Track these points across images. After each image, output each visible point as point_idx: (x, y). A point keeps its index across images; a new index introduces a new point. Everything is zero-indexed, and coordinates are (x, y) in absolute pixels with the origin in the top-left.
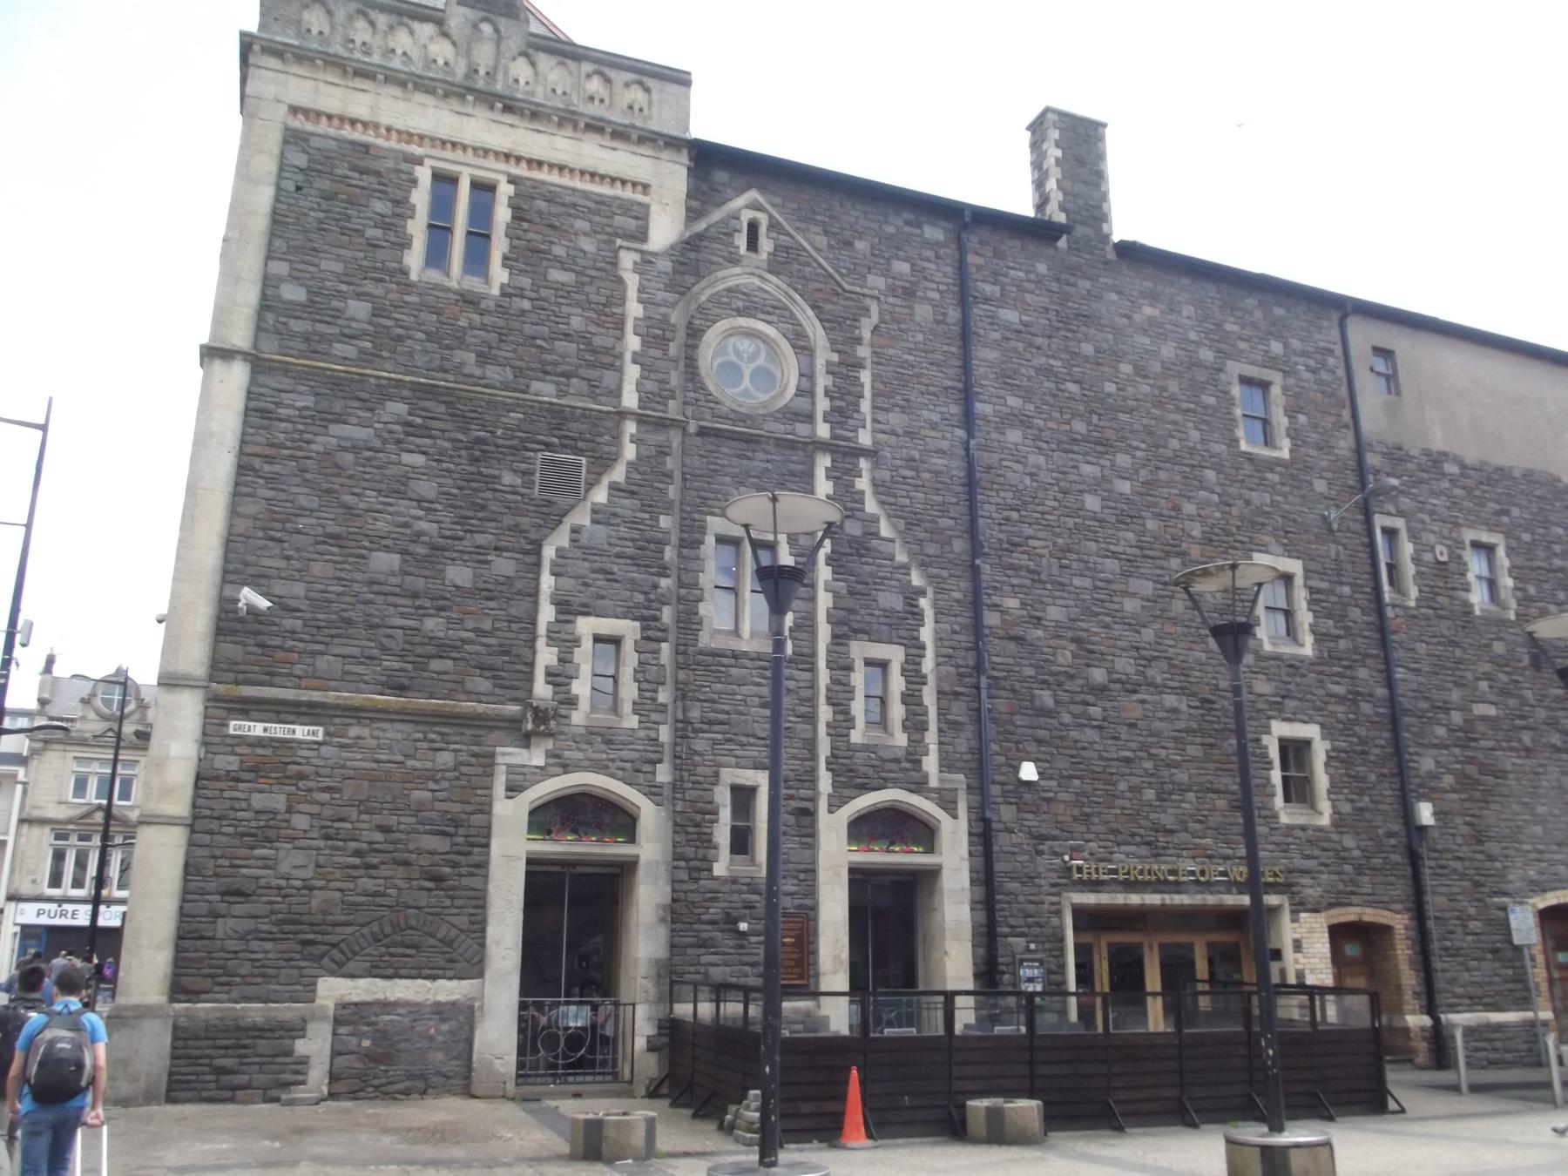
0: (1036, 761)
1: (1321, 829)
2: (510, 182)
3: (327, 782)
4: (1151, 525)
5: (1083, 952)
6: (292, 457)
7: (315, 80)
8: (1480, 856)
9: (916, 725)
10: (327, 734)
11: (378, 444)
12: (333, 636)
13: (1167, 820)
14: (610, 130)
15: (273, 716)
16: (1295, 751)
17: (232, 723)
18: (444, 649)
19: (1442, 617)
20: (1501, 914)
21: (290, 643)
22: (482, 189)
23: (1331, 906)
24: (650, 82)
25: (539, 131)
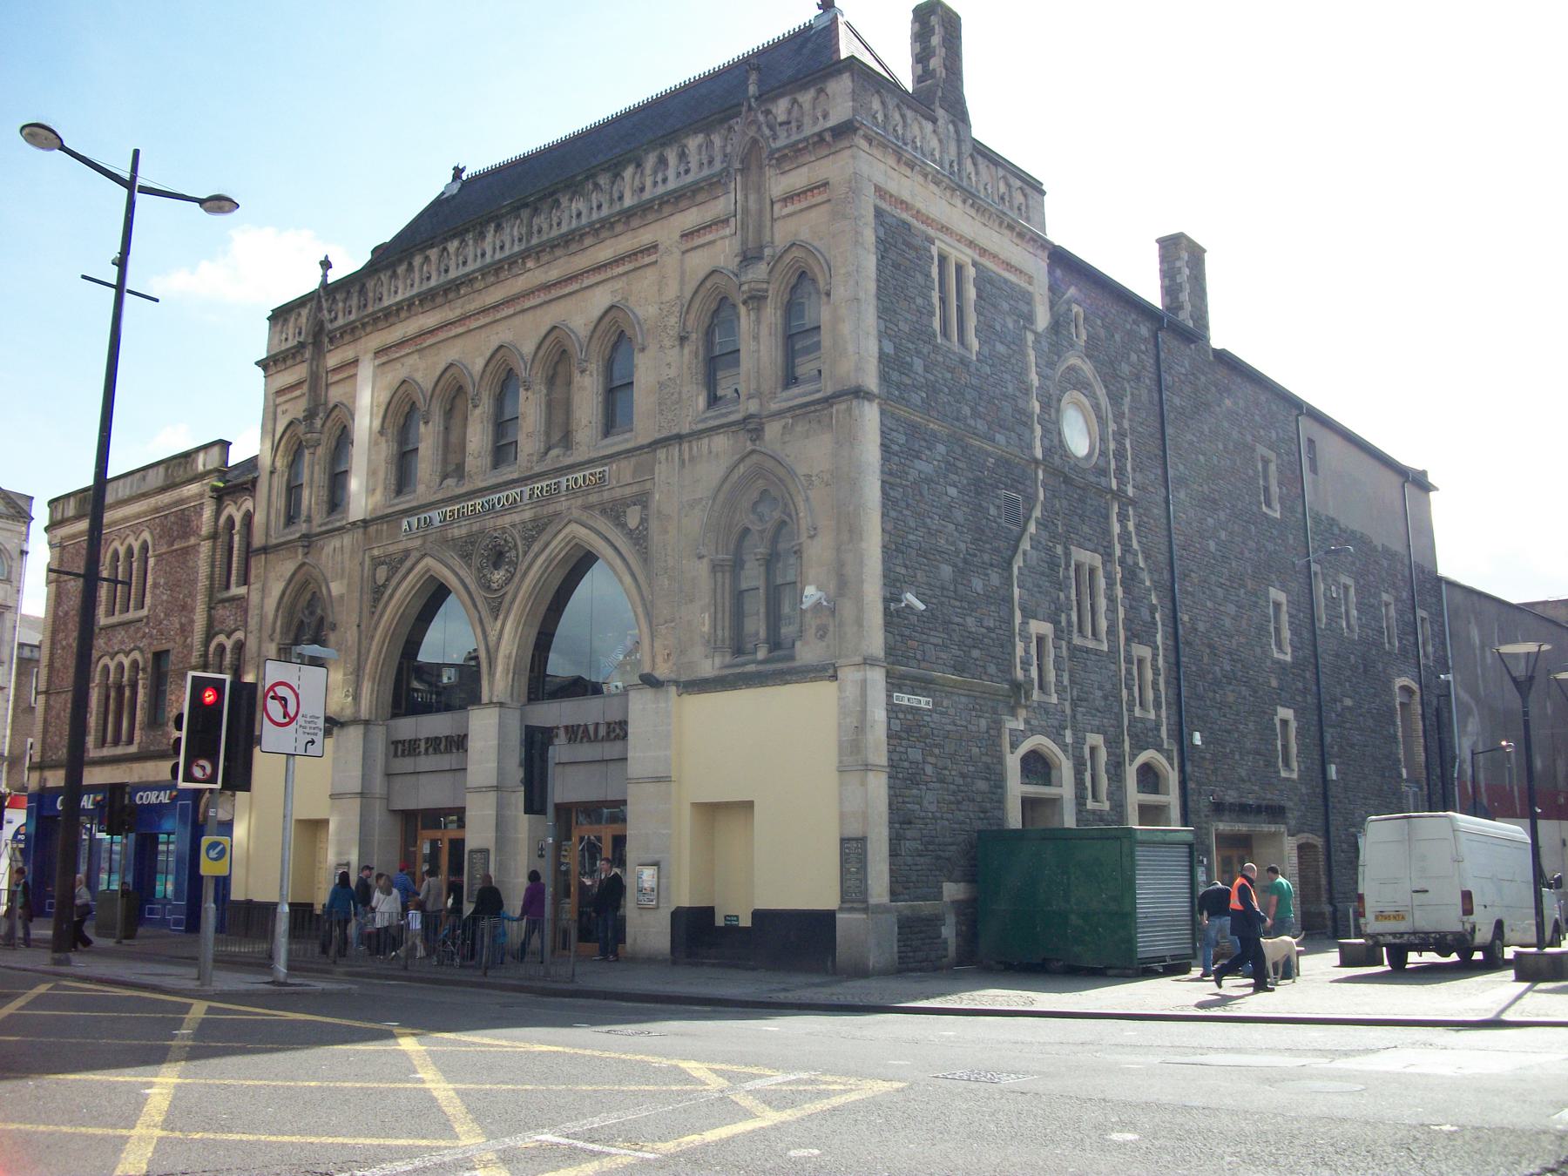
1: (1293, 781)
2: (973, 265)
9: (1157, 705)
14: (1017, 230)
16: (1285, 723)
23: (188, 547)
24: (1028, 190)
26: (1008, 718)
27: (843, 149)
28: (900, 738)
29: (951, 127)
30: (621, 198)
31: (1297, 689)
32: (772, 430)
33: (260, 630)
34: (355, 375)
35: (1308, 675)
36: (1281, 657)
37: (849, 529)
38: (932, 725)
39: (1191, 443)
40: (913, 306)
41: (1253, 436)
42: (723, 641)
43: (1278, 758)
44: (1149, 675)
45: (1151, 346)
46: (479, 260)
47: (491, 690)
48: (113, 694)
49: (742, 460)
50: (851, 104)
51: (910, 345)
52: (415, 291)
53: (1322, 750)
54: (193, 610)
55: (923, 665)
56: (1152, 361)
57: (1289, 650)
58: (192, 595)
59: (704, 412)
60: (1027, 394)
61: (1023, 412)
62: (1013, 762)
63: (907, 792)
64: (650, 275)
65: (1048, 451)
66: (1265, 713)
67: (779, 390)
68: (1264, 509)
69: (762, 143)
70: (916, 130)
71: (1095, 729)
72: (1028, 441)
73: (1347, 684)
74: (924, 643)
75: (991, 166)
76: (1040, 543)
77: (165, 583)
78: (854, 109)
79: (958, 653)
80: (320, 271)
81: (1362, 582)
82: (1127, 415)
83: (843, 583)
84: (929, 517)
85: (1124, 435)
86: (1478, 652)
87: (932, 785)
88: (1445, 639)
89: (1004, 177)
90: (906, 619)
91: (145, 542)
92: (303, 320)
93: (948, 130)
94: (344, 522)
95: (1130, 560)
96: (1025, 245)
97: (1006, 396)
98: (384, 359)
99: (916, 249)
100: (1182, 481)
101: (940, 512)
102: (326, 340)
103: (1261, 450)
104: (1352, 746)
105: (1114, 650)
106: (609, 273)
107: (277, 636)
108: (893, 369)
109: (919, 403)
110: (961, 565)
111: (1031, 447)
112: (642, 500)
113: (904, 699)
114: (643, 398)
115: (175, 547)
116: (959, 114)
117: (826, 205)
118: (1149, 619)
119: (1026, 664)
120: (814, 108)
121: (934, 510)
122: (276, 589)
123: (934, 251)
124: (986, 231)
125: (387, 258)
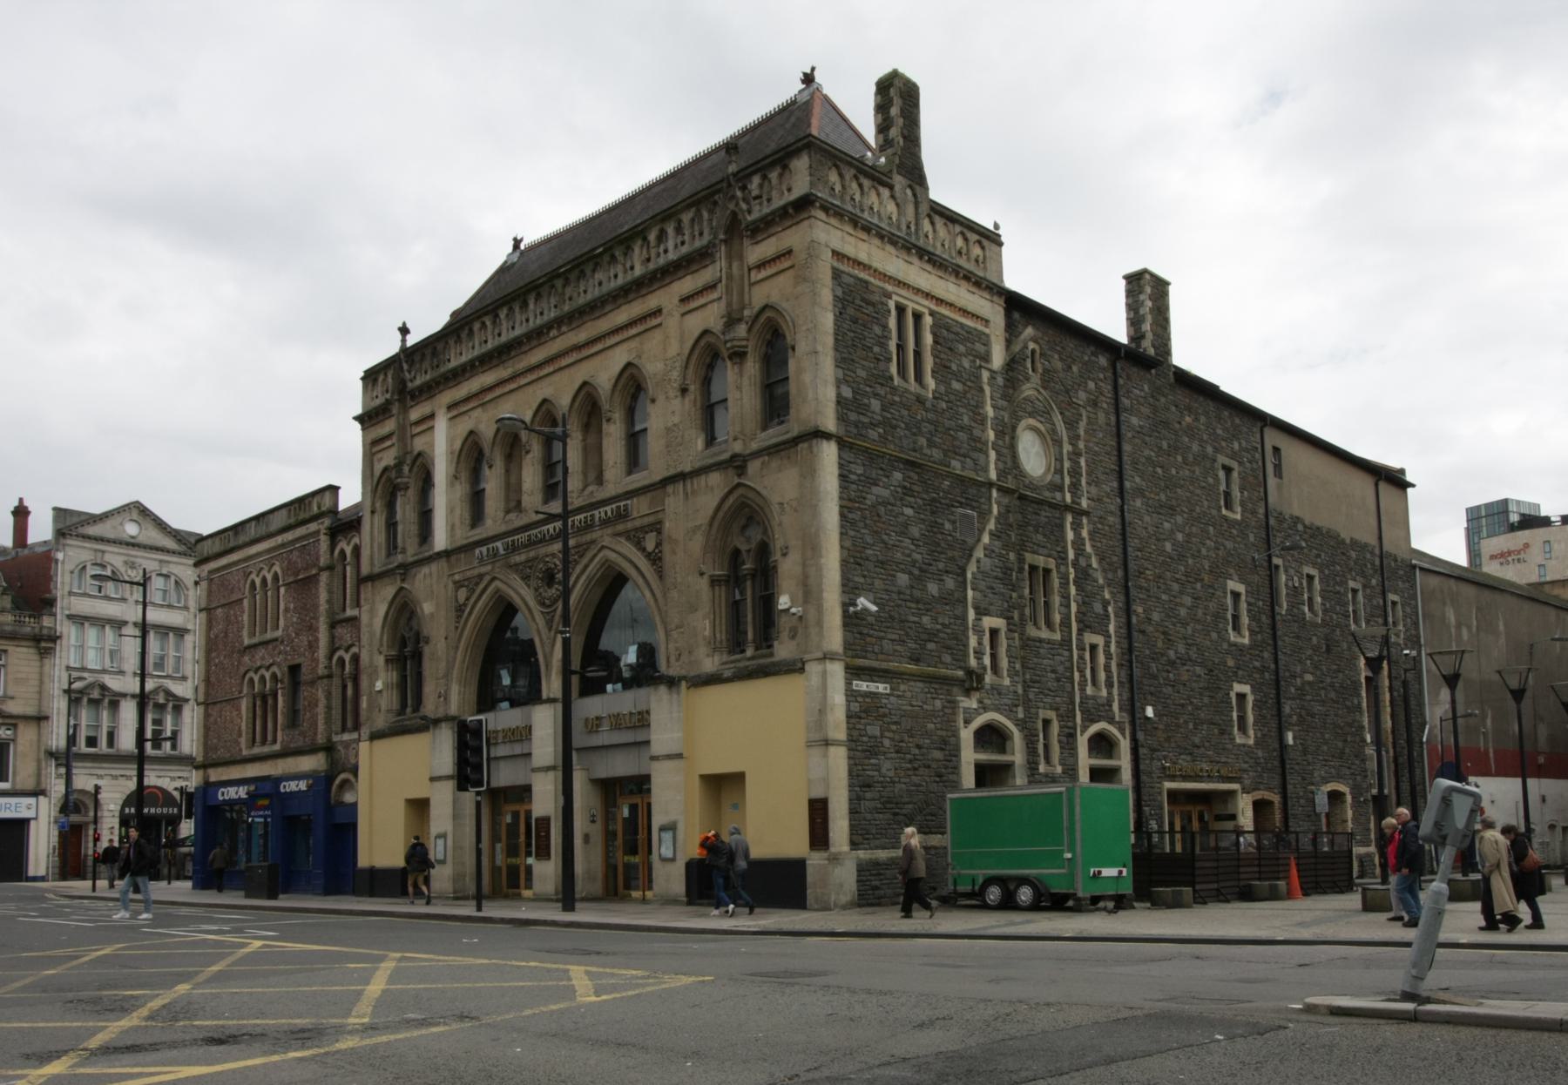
0: (1152, 705)
1: (1249, 747)
2: (930, 315)
3: (895, 719)
4: (1190, 561)
5: (1171, 814)
6: (859, 509)
7: (842, 230)
8: (1305, 763)
9: (1109, 685)
10: (891, 689)
11: (892, 500)
12: (888, 627)
13: (1197, 740)
15: (868, 677)
16: (1241, 697)
17: (854, 682)
18: (932, 636)
19: (1295, 621)
20: (1311, 795)
21: (872, 632)
22: (918, 317)
23: (1254, 790)
24: (985, 242)
25: (941, 277)
26: (962, 698)
27: (802, 220)
28: (860, 718)
29: (909, 192)
30: (632, 268)
31: (1255, 668)
32: (753, 467)
33: (370, 645)
34: (432, 427)
35: (1266, 655)
36: (1239, 640)
37: (812, 547)
38: (889, 706)
39: (1149, 459)
40: (870, 355)
41: (1215, 448)
42: (721, 642)
43: (1233, 726)
44: (1101, 659)
45: (1109, 374)
46: (524, 324)
47: (549, 689)
48: (258, 703)
49: (730, 492)
50: (808, 178)
51: (868, 389)
52: (476, 352)
53: (1280, 720)
54: (317, 630)
55: (880, 657)
56: (1109, 387)
57: (1247, 634)
58: (316, 618)
59: (702, 452)
60: (983, 425)
61: (978, 440)
62: (967, 735)
63: (866, 761)
64: (657, 335)
65: (1002, 474)
66: (1220, 689)
67: (758, 432)
68: (1224, 512)
69: (740, 217)
70: (873, 198)
71: (1048, 706)
72: (983, 465)
73: (1308, 662)
74: (881, 638)
75: (949, 223)
76: (993, 551)
77: (295, 608)
78: (812, 184)
79: (914, 646)
80: (399, 337)
81: (1327, 572)
82: (1082, 438)
83: (809, 592)
84: (886, 534)
85: (1079, 454)
86: (1453, 630)
87: (889, 756)
88: (1418, 619)
89: (962, 233)
90: (864, 619)
91: (276, 574)
92: (390, 380)
93: (905, 194)
94: (431, 553)
95: (1083, 562)
96: (981, 293)
97: (962, 428)
98: (455, 413)
99: (873, 305)
100: (1140, 492)
101: (897, 529)
102: (409, 397)
103: (1222, 459)
104: (1313, 716)
105: (1066, 642)
106: (626, 334)
107: (384, 649)
108: (852, 411)
109: (876, 438)
110: (916, 572)
111: (986, 470)
112: (657, 527)
113: (862, 686)
114: (654, 446)
115: (301, 577)
116: (916, 177)
117: (791, 271)
118: (1102, 612)
119: (979, 654)
120: (780, 183)
121: (891, 528)
122: (382, 609)
123: (892, 305)
124: (942, 283)
125: (462, 324)
